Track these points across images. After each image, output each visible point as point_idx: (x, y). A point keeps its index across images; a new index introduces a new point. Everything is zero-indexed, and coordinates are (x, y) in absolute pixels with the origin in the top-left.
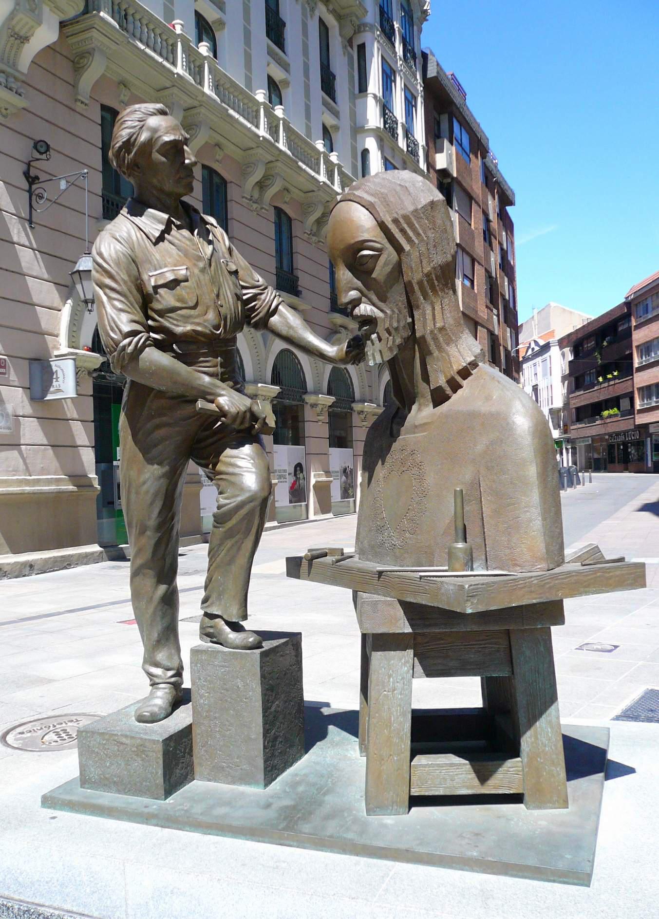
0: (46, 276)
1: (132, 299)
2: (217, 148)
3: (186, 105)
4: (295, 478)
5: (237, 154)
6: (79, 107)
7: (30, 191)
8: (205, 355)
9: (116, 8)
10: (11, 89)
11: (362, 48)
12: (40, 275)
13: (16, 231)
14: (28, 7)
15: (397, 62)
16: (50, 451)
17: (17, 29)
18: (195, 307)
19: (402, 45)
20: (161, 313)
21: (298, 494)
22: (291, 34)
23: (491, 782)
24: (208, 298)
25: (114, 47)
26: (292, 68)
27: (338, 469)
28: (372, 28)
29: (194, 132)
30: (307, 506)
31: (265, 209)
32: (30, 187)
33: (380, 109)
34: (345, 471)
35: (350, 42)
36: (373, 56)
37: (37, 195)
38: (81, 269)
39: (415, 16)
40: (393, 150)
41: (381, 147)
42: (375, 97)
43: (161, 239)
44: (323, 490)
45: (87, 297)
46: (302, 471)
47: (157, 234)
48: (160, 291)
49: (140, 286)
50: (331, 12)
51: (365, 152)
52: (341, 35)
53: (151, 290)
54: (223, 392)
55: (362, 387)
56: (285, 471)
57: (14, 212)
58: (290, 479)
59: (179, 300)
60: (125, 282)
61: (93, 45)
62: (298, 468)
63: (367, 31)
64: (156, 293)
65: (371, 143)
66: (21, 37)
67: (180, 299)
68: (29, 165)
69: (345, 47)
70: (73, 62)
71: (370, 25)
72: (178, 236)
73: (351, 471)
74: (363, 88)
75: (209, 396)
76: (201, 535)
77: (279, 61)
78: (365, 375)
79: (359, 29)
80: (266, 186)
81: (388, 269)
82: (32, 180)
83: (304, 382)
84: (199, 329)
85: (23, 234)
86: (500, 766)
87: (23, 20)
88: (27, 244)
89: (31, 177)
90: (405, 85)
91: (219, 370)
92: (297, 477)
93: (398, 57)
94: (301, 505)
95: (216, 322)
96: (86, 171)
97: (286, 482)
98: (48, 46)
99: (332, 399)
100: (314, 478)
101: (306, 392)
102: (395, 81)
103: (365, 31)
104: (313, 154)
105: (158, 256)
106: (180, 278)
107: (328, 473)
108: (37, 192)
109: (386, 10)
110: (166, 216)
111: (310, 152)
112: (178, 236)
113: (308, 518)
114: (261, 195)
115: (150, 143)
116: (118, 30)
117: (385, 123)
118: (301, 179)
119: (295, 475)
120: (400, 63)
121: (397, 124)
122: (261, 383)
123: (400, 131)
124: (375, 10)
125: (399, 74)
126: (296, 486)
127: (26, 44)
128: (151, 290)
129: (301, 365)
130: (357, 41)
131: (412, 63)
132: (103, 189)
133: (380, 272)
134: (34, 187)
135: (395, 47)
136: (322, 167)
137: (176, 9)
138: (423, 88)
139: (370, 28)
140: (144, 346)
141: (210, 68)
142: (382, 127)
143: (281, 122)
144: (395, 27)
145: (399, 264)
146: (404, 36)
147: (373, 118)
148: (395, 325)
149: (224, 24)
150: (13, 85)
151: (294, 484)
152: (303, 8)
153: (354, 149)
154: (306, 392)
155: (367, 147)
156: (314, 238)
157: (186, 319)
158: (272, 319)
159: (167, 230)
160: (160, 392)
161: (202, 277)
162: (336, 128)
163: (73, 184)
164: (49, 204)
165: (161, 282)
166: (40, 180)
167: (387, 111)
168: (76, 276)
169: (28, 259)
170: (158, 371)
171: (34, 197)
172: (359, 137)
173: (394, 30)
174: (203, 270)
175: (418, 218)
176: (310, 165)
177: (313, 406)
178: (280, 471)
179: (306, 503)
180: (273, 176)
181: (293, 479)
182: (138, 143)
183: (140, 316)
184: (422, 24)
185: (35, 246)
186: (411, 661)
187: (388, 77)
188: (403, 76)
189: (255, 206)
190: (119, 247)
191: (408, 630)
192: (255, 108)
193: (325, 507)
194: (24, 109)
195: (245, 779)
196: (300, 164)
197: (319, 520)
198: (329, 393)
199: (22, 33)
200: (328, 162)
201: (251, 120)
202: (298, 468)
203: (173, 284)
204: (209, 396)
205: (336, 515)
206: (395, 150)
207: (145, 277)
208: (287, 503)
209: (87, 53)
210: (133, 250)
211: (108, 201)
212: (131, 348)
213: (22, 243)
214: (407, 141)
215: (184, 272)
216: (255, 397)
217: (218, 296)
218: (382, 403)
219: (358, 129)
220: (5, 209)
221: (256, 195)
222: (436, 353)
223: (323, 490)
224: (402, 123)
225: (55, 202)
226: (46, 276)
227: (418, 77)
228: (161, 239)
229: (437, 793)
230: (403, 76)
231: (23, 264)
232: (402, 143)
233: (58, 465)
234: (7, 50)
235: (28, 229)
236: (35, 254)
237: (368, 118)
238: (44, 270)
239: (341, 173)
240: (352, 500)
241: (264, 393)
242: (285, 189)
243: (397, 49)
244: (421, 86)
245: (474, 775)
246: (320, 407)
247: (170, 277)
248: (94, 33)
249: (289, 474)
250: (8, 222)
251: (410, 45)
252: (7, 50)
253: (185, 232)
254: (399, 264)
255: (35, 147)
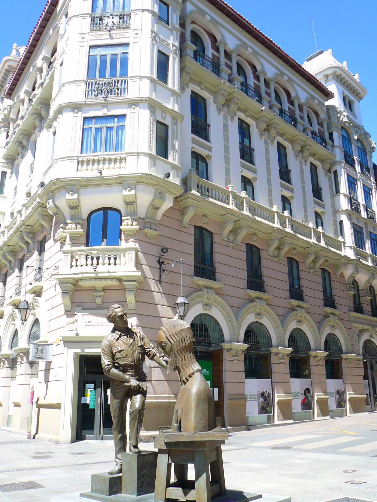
0: (166, 304)
1: (109, 356)
2: (253, 235)
3: (235, 220)
4: (305, 396)
5: (265, 236)
6: (184, 229)
7: (160, 269)
8: (129, 370)
9: (200, 187)
10: (152, 229)
11: (335, 172)
12: (164, 304)
13: (153, 286)
14: (159, 196)
15: (357, 175)
16: (166, 383)
17: (155, 205)
18: (126, 357)
19: (359, 166)
20: (117, 359)
21: (340, 404)
22: (295, 175)
23: (188, 496)
24: (130, 354)
25: (198, 203)
26: (295, 191)
27: (333, 391)
28: (340, 163)
29: (240, 230)
30: (313, 412)
31: (282, 260)
32: (160, 267)
33: (348, 200)
34: (338, 392)
35: (329, 171)
36: (342, 175)
37: (163, 270)
38: (178, 302)
39: (367, 151)
40: (358, 219)
41: (350, 218)
42: (344, 194)
43: (118, 339)
44: (323, 404)
45: (181, 314)
46: (309, 392)
47: (117, 338)
48: (117, 353)
49: (112, 352)
50: (317, 159)
51: (341, 222)
52: (323, 169)
53: (114, 353)
54: (131, 380)
55: (347, 345)
56: (298, 393)
57: (153, 278)
58: (302, 397)
59: (121, 356)
60: (107, 352)
61: (189, 204)
62: (307, 391)
63: (338, 164)
64: (116, 354)
65: (344, 218)
66: (157, 208)
67: (122, 355)
68: (160, 257)
69: (326, 174)
70: (181, 211)
71: (339, 161)
72: (123, 338)
73: (343, 392)
74: (338, 191)
75: (128, 381)
76: (246, 426)
77: (287, 189)
78: (348, 338)
79: (334, 163)
80: (281, 249)
81: (169, 348)
82: (161, 263)
83: (308, 343)
84: (127, 363)
85: (156, 287)
86: (190, 491)
87: (157, 202)
88: (158, 291)
89: (161, 262)
90: (363, 184)
91: (133, 374)
92: (306, 396)
93: (358, 173)
94: (310, 411)
95: (132, 361)
96: (182, 260)
97: (299, 398)
98: (171, 207)
99: (326, 353)
100: (317, 395)
101: (310, 350)
102: (357, 184)
103: (336, 164)
104: (307, 230)
105: (117, 344)
106: (122, 350)
107: (325, 393)
108: (163, 268)
109: (348, 152)
110: (120, 333)
111: (305, 229)
112: (123, 338)
113: (314, 419)
114: (279, 254)
115: (115, 315)
116: (200, 197)
117: (352, 206)
118: (300, 243)
119: (305, 394)
120: (359, 175)
121: (360, 205)
122: (280, 347)
123: (362, 208)
124: (341, 154)
125: (359, 181)
126: (306, 401)
127: (159, 210)
128: (114, 353)
129: (306, 335)
130: (333, 170)
131: (367, 173)
132: (195, 262)
133: (167, 349)
134: (162, 266)
135: (355, 168)
136: (313, 235)
137: (231, 179)
138: (376, 184)
139: (339, 163)
140: (111, 368)
141: (246, 202)
142: (350, 208)
143: (287, 218)
144: (355, 159)
145: (172, 347)
146: (361, 161)
147: (344, 204)
148: (173, 363)
149: (257, 179)
150: (153, 227)
151: (304, 399)
152: (300, 161)
153: (335, 222)
154: (310, 350)
155: (341, 219)
156: (312, 270)
157: (124, 361)
158: (155, 357)
159: (120, 337)
160: (117, 380)
161: (128, 349)
162: (324, 213)
163: (171, 271)
164: (168, 272)
165: (116, 351)
166: (165, 263)
167: (352, 200)
168: (176, 305)
169: (159, 298)
170: (115, 375)
171: (162, 271)
172: (337, 215)
173: (354, 160)
174: (129, 347)
175: (177, 335)
176: (306, 235)
177: (315, 357)
178: (295, 393)
179: (313, 410)
180: (284, 244)
181: (303, 397)
182: (112, 316)
183: (111, 360)
184: (372, 153)
185: (162, 292)
186: (167, 457)
187: (352, 183)
188: (361, 181)
189: (276, 259)
190: (107, 342)
191: (165, 448)
192: (272, 215)
193: (325, 411)
194: (159, 235)
195: (132, 494)
196: (299, 236)
197: (320, 420)
198: (325, 350)
199: (157, 206)
200: (316, 232)
201: (270, 220)
202: (307, 391)
203: (120, 351)
204: (128, 381)
205: (332, 417)
206: (359, 219)
207: (113, 350)
208: (300, 410)
209: (187, 207)
210: (110, 343)
211: (197, 268)
212: (107, 369)
213: (156, 291)
214: (367, 212)
215: (123, 348)
216: (277, 354)
217: (133, 354)
218: (361, 353)
219: (336, 211)
220: (149, 277)
221: (276, 254)
222: (182, 371)
223: (323, 404)
224: (363, 204)
225: (171, 271)
226: (166, 304)
227: (372, 179)
228: (118, 339)
229: (173, 498)
230: (361, 181)
231: (156, 300)
232: (364, 214)
233: (169, 390)
234: (151, 213)
235: (159, 285)
236: (161, 295)
237: (341, 205)
238: (166, 301)
239: (324, 236)
240: (344, 408)
241: (282, 352)
242: (293, 248)
243: (357, 169)
244: (374, 183)
245: (183, 494)
246: (319, 357)
247: (120, 349)
248: (189, 200)
249: (301, 394)
250: (150, 283)
251: (365, 165)
252: (151, 213)
253: (125, 337)
254: (172, 347)
255: (162, 251)
